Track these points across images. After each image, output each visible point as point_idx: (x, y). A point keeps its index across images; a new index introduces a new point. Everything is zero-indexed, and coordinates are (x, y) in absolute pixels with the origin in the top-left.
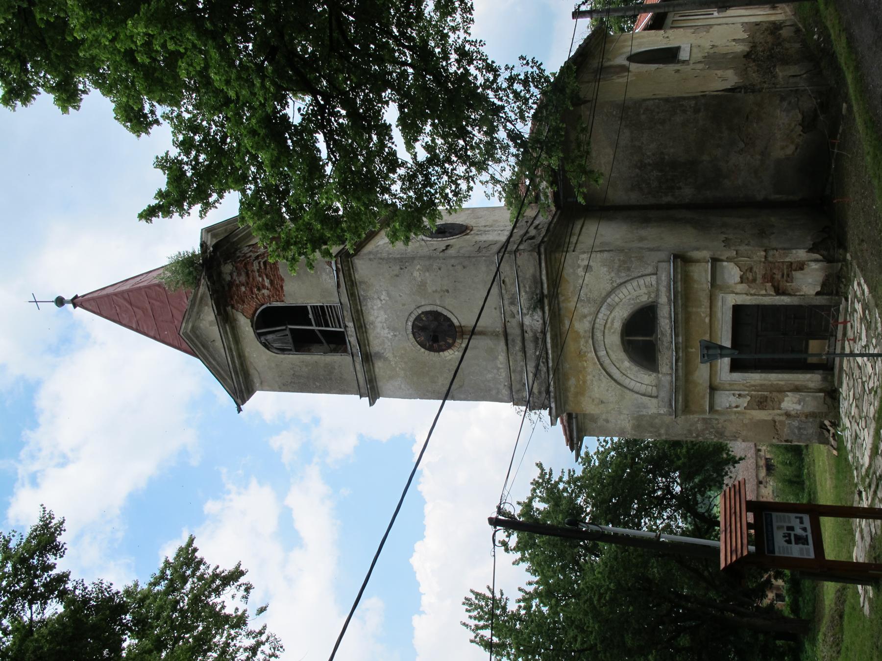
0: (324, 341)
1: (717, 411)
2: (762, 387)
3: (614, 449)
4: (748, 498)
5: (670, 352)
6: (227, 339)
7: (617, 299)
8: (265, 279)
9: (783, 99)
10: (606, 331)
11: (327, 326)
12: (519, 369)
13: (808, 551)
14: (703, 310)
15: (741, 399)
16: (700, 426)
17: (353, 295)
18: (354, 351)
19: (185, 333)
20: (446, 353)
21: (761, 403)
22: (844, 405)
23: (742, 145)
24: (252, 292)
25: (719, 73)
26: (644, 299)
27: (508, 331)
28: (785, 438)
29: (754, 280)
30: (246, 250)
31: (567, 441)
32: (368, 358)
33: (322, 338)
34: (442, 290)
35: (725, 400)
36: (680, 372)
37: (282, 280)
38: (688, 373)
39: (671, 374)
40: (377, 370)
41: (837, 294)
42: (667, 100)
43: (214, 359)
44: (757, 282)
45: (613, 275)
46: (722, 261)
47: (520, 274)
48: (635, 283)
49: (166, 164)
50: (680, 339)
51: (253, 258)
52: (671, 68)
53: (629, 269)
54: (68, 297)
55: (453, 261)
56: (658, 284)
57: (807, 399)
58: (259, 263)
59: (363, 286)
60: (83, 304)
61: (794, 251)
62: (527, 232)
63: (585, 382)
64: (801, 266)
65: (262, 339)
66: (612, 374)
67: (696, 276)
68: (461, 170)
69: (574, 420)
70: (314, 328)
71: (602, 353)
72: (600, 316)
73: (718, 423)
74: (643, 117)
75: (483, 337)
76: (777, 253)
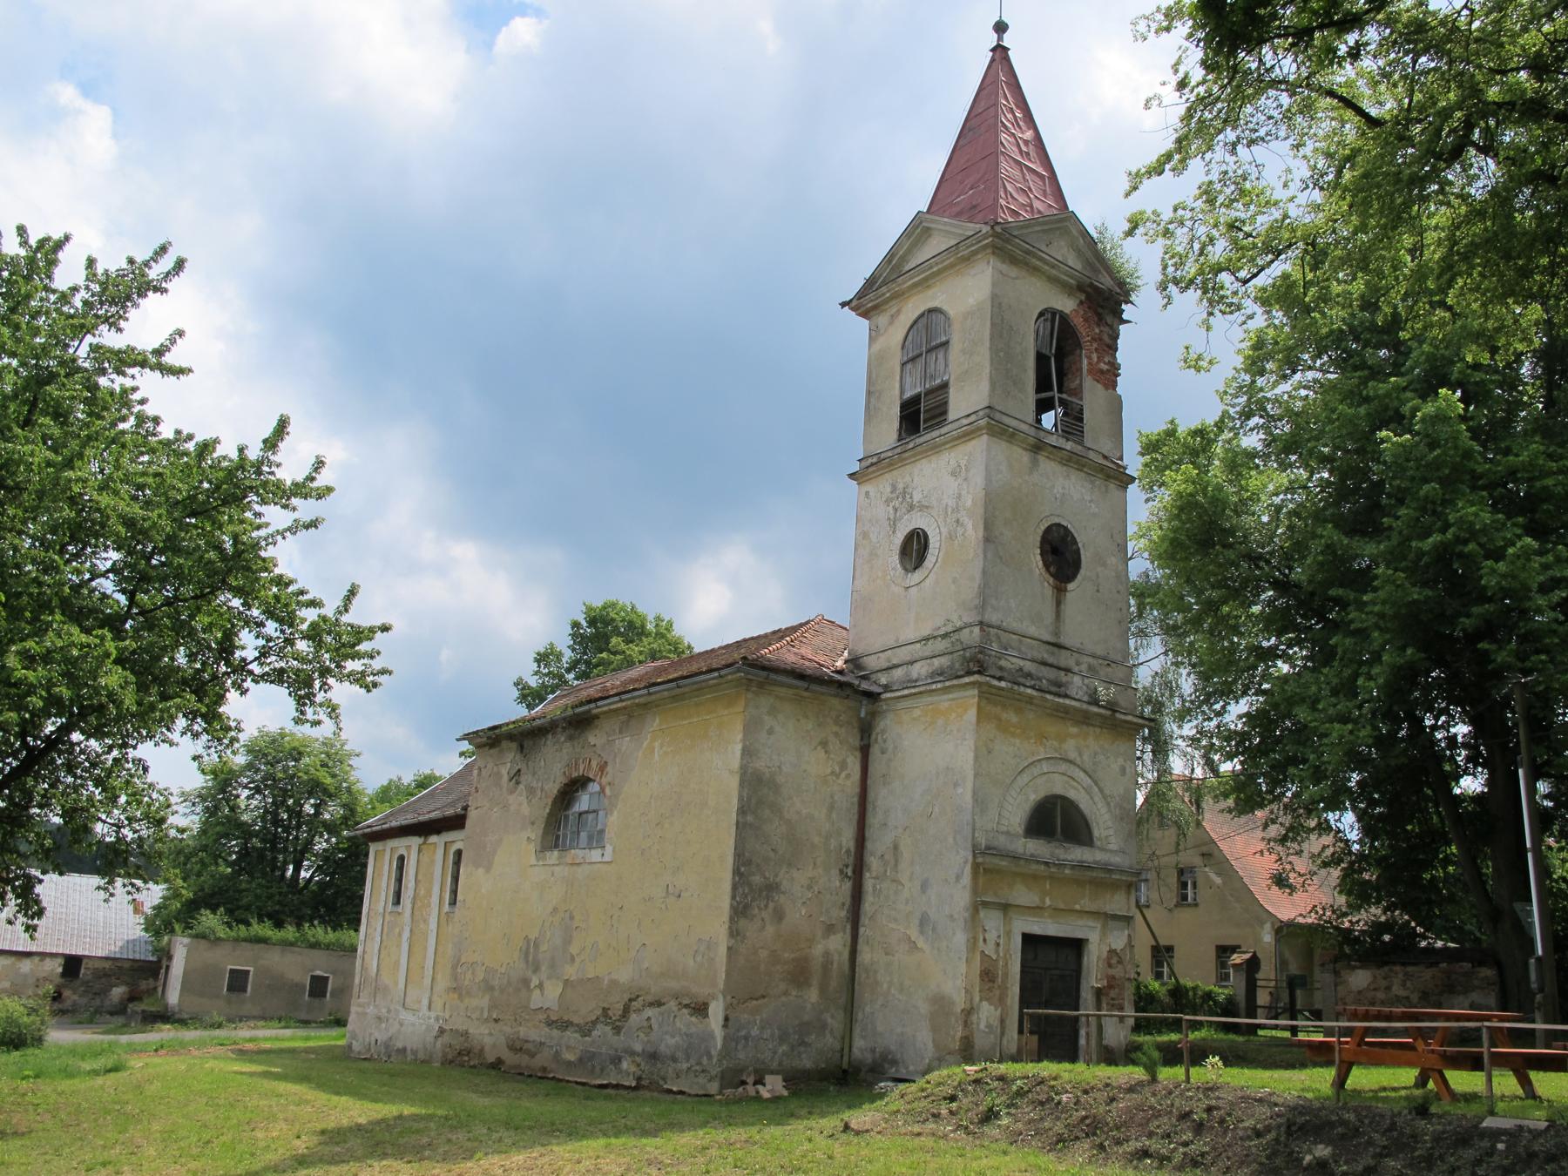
2: (1006, 975)
10: (1065, 778)
12: (1023, 649)
20: (1039, 558)
26: (1096, 833)
27: (1063, 651)
63: (1013, 735)
71: (1045, 767)
72: (1082, 775)
73: (760, 909)
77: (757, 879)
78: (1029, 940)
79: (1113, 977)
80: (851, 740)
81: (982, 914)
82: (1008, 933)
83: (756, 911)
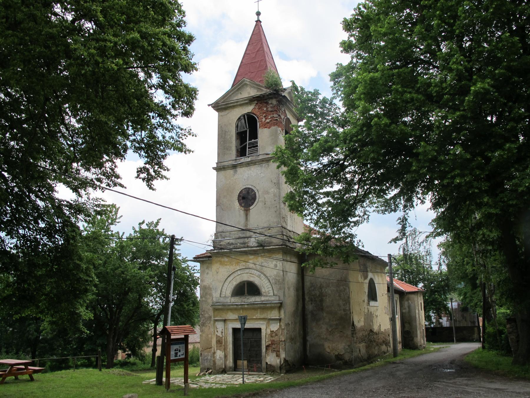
0: (242, 146)
1: (215, 323)
2: (226, 342)
3: (190, 274)
4: (189, 336)
6: (242, 101)
7: (263, 279)
9: (349, 346)
10: (249, 274)
11: (249, 148)
13: (173, 357)
14: (259, 315)
16: (207, 315)
17: (263, 161)
18: (238, 161)
19: (244, 81)
21: (219, 342)
22: (220, 376)
23: (330, 330)
24: (263, 113)
25: (363, 319)
26: (263, 290)
28: (202, 353)
29: (272, 337)
30: (283, 109)
31: (198, 256)
32: (234, 167)
33: (244, 145)
34: (265, 202)
35: (220, 326)
36: (232, 307)
37: (269, 128)
38: (231, 310)
39: (231, 303)
40: (229, 171)
41: (267, 371)
42: (349, 297)
43: (232, 94)
45: (273, 277)
46: (280, 323)
48: (270, 286)
49: (316, 93)
50: (246, 306)
51: (279, 114)
52: (366, 298)
53: (276, 283)
54: (261, 18)
55: (278, 206)
56: (270, 296)
58: (277, 117)
59: (267, 166)
60: (257, 26)
61: (284, 352)
62: (291, 238)
63: (226, 265)
64: (278, 356)
65: (242, 117)
67: (273, 312)
68: (315, 217)
69: (208, 259)
70: (248, 142)
71: (239, 272)
72: (256, 271)
74: (342, 288)
75: (245, 220)
76: (283, 345)
79: (274, 341)
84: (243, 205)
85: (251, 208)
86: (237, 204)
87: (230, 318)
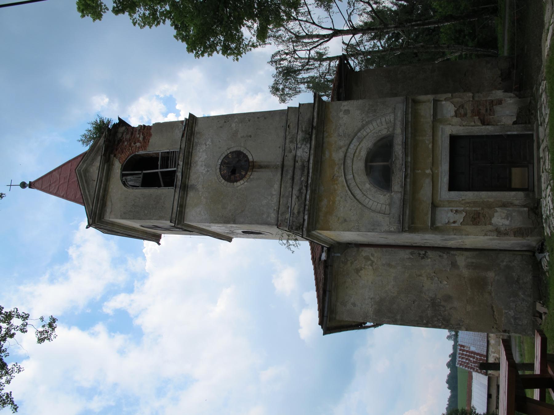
2: (475, 203)
5: (402, 173)
8: (141, 135)
10: (355, 159)
12: (287, 194)
15: (458, 215)
26: (385, 132)
27: (285, 163)
29: (465, 115)
40: (188, 199)
41: (530, 123)
44: (468, 116)
45: (363, 115)
46: (442, 101)
47: (300, 118)
50: (409, 159)
56: (395, 119)
57: (514, 214)
61: (494, 92)
64: (500, 102)
66: (356, 195)
71: (350, 177)
72: (352, 146)
73: (445, 311)
77: (430, 313)
78: (452, 187)
79: (473, 111)
80: (354, 254)
81: (438, 224)
82: (450, 202)
83: (446, 313)
84: (243, 173)
85: (250, 158)
86: (240, 184)
87: (430, 195)
